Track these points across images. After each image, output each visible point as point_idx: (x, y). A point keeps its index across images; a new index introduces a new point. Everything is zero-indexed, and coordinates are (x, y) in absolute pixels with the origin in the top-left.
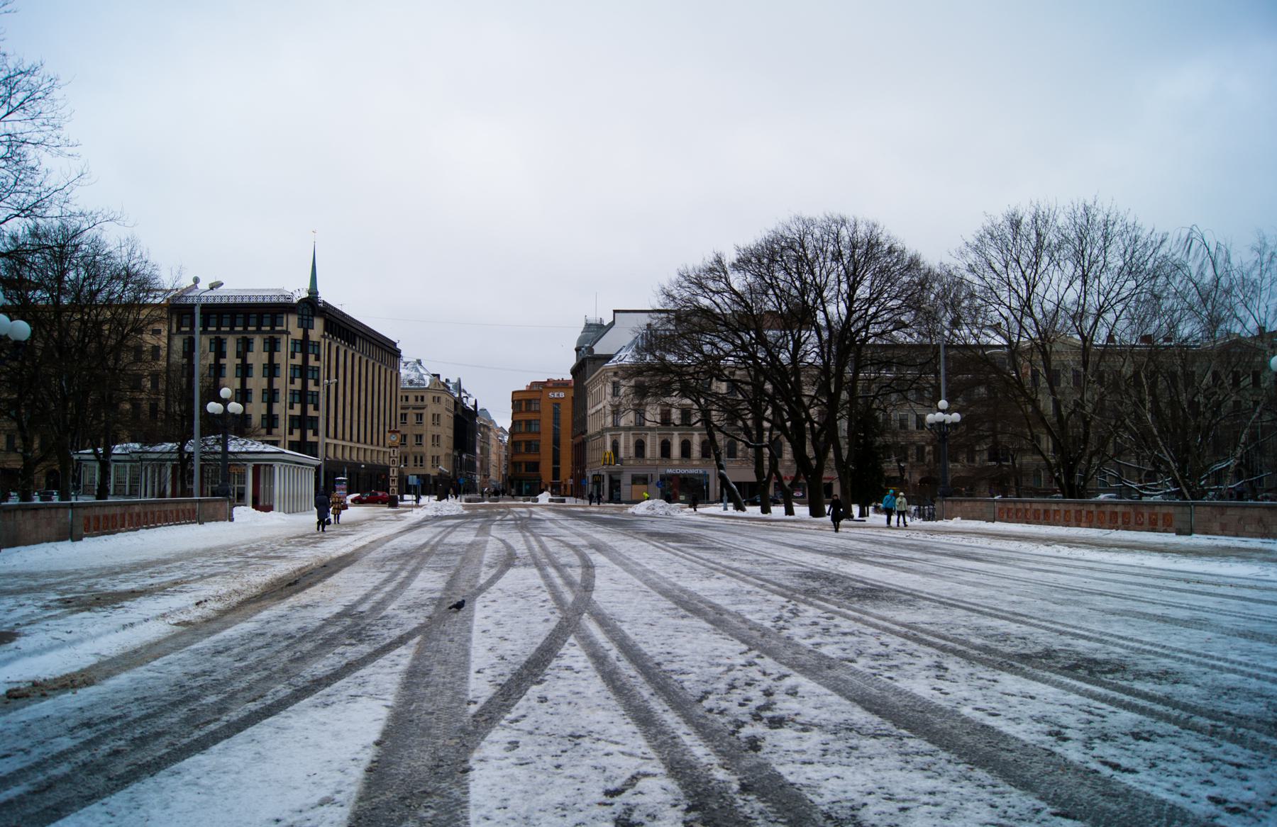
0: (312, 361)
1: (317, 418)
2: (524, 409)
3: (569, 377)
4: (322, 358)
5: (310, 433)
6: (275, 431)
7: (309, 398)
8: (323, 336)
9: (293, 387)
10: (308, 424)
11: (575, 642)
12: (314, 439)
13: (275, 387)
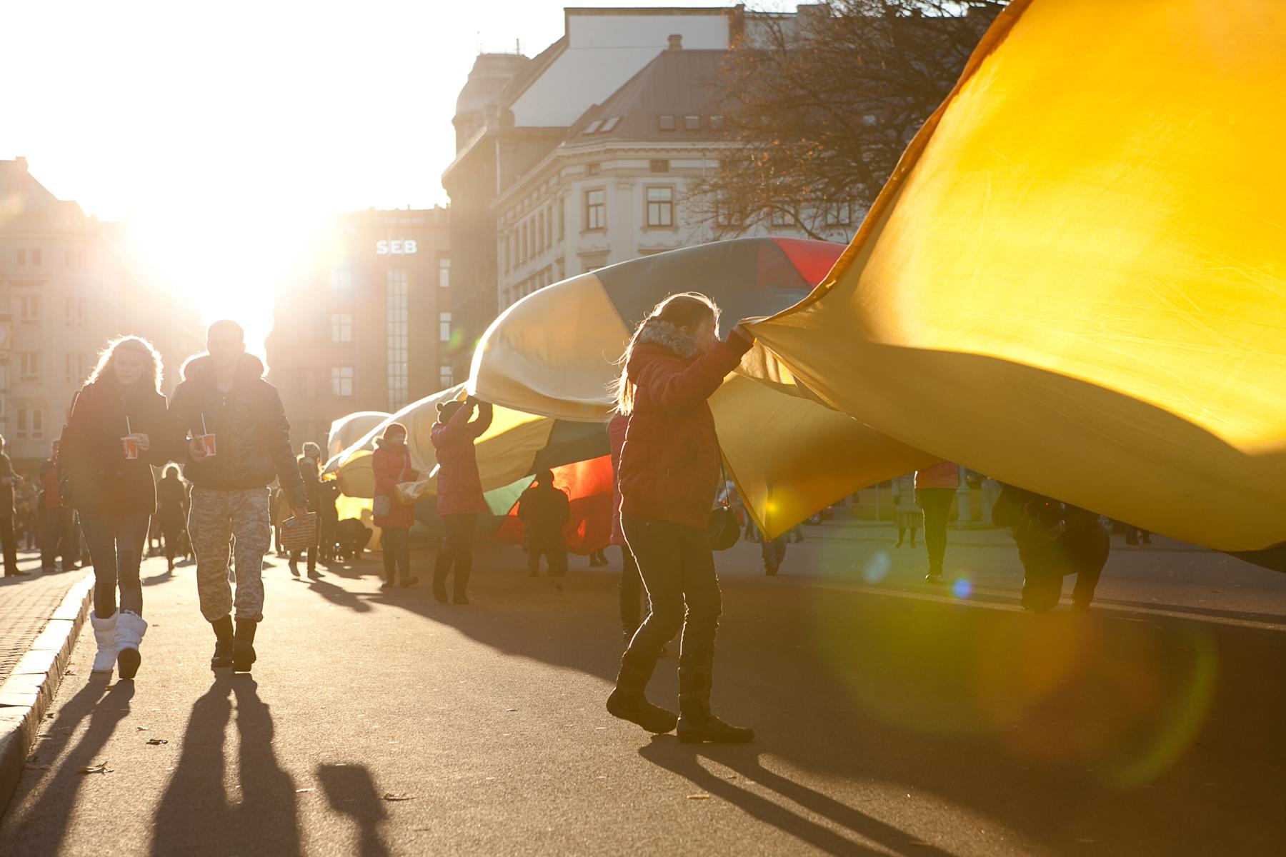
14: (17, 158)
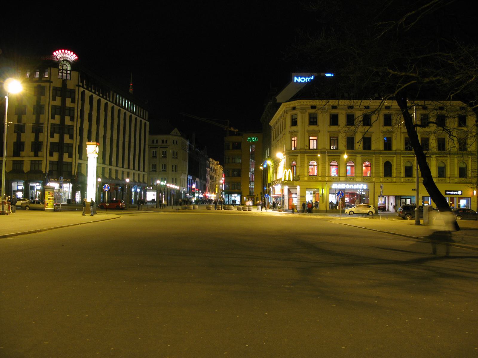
0: (68, 103)
1: (72, 127)
2: (332, 139)
3: (420, 220)
4: (76, 101)
5: (67, 119)
6: (40, 154)
7: (67, 112)
8: (78, 86)
9: (53, 122)
10: (65, 149)
11: (430, 115)
12: (69, 160)
13: (40, 140)
14: (24, 142)
